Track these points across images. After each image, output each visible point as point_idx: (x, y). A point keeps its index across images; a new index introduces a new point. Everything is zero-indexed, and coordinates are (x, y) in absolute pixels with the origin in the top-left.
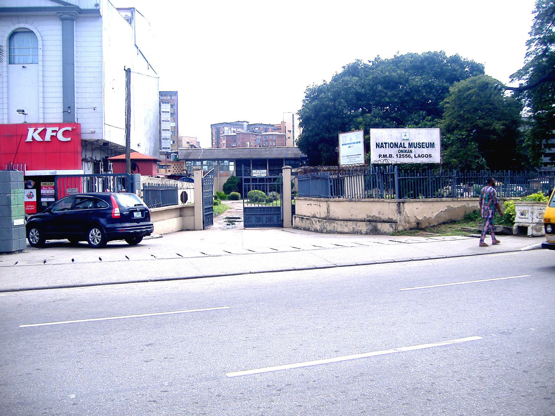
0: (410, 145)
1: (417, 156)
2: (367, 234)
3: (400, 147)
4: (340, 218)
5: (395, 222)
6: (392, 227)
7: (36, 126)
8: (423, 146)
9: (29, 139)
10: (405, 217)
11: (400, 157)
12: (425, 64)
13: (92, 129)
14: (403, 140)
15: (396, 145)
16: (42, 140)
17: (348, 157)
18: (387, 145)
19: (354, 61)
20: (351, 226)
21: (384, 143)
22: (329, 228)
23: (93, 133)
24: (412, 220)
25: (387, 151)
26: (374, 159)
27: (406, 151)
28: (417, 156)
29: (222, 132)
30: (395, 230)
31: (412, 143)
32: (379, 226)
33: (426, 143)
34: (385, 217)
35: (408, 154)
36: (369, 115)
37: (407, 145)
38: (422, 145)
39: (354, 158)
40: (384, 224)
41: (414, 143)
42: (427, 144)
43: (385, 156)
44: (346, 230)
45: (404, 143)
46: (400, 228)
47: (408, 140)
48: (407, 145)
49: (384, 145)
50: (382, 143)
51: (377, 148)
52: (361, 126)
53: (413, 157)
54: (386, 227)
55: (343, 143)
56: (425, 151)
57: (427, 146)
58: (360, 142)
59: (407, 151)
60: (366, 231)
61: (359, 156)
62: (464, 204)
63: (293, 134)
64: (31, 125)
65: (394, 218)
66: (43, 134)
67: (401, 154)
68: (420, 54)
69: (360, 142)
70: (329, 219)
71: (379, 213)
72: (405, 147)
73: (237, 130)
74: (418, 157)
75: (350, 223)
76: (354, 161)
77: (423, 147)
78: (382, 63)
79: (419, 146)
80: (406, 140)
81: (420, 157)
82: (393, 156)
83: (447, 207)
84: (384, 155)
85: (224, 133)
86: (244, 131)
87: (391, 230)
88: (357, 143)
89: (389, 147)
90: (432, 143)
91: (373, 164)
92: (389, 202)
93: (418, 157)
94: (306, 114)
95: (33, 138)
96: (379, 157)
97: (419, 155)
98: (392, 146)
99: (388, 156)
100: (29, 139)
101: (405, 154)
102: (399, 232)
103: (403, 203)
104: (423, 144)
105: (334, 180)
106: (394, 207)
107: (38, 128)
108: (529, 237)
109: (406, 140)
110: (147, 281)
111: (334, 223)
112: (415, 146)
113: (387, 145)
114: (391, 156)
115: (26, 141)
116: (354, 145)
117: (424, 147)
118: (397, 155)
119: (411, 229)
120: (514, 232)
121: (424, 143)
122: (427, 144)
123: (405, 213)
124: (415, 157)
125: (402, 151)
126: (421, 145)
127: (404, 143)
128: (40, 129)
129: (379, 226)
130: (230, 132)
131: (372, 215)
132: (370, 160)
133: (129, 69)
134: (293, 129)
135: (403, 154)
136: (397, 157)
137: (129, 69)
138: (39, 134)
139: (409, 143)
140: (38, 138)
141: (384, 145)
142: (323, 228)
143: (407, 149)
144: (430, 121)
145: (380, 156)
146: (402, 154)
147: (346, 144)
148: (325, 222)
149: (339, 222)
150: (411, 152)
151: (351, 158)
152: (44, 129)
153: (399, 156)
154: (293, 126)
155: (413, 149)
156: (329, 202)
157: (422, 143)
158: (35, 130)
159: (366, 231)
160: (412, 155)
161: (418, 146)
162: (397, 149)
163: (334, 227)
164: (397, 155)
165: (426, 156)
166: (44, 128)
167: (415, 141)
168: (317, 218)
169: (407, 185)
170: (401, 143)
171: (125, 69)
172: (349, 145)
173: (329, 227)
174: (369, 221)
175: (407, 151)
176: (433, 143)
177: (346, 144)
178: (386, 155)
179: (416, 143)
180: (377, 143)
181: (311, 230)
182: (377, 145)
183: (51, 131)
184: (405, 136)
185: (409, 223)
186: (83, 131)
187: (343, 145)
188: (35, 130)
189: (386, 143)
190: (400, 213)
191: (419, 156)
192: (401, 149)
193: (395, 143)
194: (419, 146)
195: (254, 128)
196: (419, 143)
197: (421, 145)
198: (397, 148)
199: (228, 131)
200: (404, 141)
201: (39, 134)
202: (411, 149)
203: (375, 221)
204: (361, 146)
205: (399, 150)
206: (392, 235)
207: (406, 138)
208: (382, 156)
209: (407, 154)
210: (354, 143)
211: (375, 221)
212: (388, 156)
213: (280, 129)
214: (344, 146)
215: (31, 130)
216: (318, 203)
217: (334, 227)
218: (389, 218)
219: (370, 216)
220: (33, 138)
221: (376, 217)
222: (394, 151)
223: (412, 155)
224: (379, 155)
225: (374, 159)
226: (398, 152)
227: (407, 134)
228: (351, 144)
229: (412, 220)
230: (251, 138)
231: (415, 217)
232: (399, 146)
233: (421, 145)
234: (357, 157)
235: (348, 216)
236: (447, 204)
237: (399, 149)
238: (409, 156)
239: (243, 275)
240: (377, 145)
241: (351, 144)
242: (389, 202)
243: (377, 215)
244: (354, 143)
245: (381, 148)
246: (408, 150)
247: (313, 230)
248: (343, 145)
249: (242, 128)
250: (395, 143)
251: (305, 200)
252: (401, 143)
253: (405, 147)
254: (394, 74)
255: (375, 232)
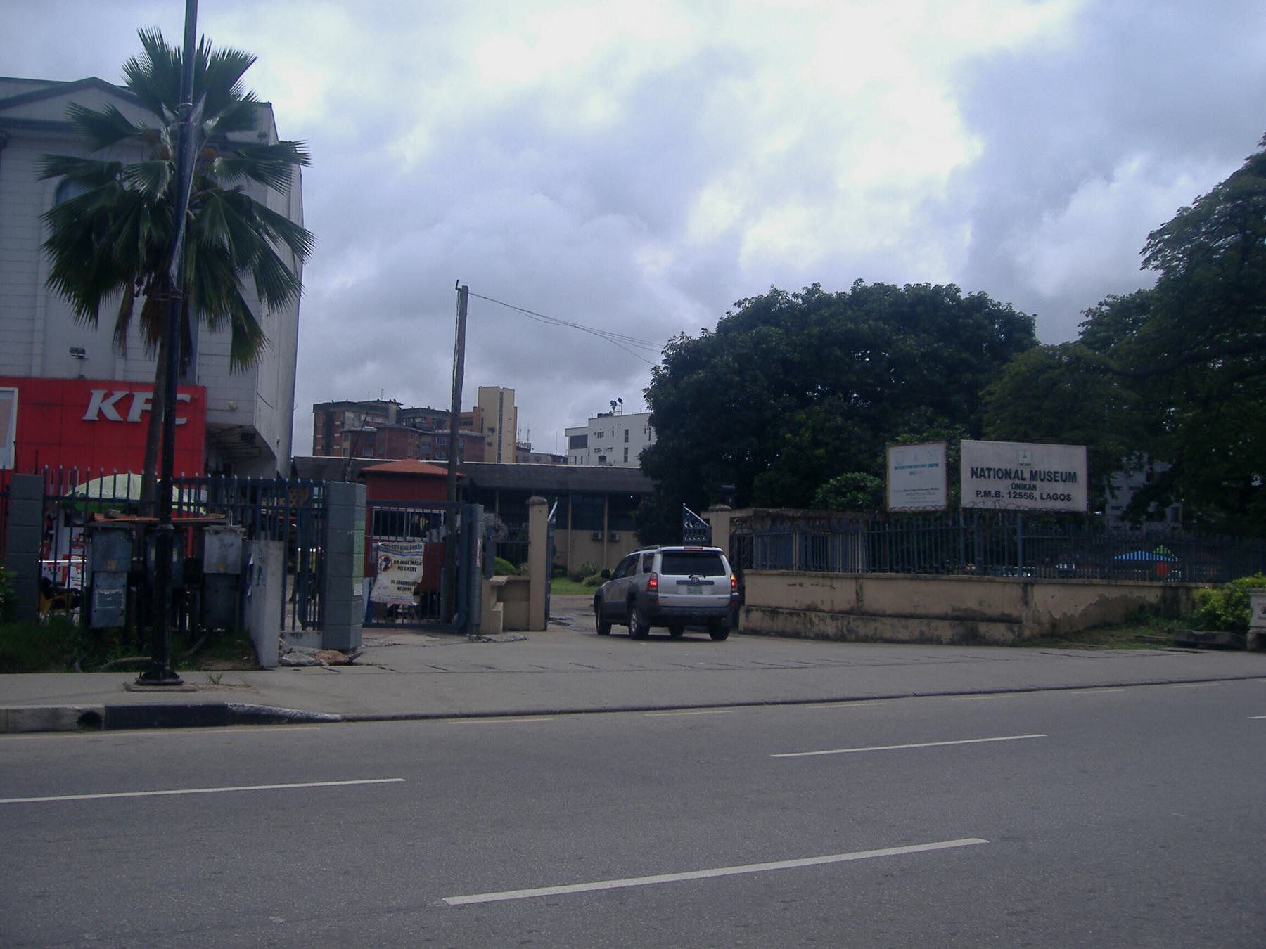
0: (1034, 475)
1: (1045, 497)
2: (953, 643)
3: (1015, 477)
4: (889, 612)
5: (1018, 621)
6: (1013, 631)
7: (109, 386)
8: (1057, 478)
9: (91, 414)
10: (1034, 612)
11: (1014, 497)
12: (920, 309)
13: (231, 402)
14: (1021, 464)
15: (1007, 474)
16: (122, 420)
17: (909, 492)
18: (992, 473)
19: (766, 292)
20: (915, 627)
21: (987, 469)
22: (862, 631)
23: (232, 410)
24: (1045, 618)
25: (992, 485)
26: (967, 499)
27: (1025, 487)
28: (1045, 497)
29: (339, 423)
30: (1019, 636)
31: (1036, 471)
32: (983, 628)
33: (1062, 473)
34: (994, 611)
35: (1029, 492)
36: (817, 408)
37: (1026, 475)
38: (1055, 477)
39: (922, 494)
40: (992, 626)
41: (1040, 472)
42: (1042, 473)
43: (987, 494)
44: (904, 635)
45: (1022, 471)
46: (1027, 633)
47: (1030, 465)
48: (1026, 475)
49: (986, 473)
50: (982, 470)
51: (972, 477)
52: (803, 429)
53: (1039, 498)
54: (999, 631)
55: (897, 465)
56: (1059, 488)
57: (1064, 478)
58: (937, 465)
59: (1027, 486)
60: (951, 637)
61: (933, 491)
62: (1126, 592)
63: (500, 437)
64: (98, 384)
65: (1015, 613)
66: (124, 405)
67: (1016, 491)
68: (901, 287)
69: (937, 465)
70: (860, 612)
71: (981, 603)
72: (1024, 479)
73: (373, 419)
74: (1047, 498)
75: (913, 623)
76: (919, 502)
77: (1056, 481)
78: (827, 301)
79: (1049, 479)
80: (1026, 465)
81: (1050, 498)
82: (1001, 495)
83: (1100, 595)
84: (985, 492)
85: (343, 424)
86: (392, 421)
87: (1010, 637)
88: (931, 466)
89: (994, 478)
90: (1034, 472)
91: (963, 508)
92: (1005, 583)
93: (1047, 498)
94: (672, 398)
95: (100, 413)
96: (977, 496)
97: (1049, 495)
98: (1000, 475)
99: (993, 493)
100: (91, 414)
101: (1023, 491)
102: (1024, 640)
103: (1032, 584)
104: (1057, 475)
105: (823, 538)
106: (1016, 592)
107: (114, 392)
108: (547, 581)
109: (1026, 465)
110: (762, 704)
111: (875, 620)
112: (1042, 477)
113: (992, 473)
114: (998, 494)
115: (84, 418)
116: (923, 469)
117: (1058, 481)
118: (1009, 493)
119: (1043, 636)
120: (1248, 645)
121: (1058, 472)
122: (1042, 473)
123: (1033, 605)
124: (1042, 498)
125: (1018, 486)
126: (1052, 475)
127: (1022, 471)
128: (119, 395)
129: (983, 628)
130: (357, 423)
131: (964, 606)
132: (959, 499)
133: (465, 288)
134: (501, 424)
135: (1021, 491)
136: (1010, 497)
137: (465, 288)
138: (116, 405)
139: (1031, 472)
140: (112, 414)
141: (986, 473)
142: (848, 631)
143: (1028, 482)
144: (946, 427)
145: (978, 493)
146: (1018, 491)
147: (903, 468)
148: (854, 620)
149: (888, 621)
150: (1034, 488)
151: (914, 494)
152: (127, 395)
153: (1012, 495)
154: (501, 420)
155: (1038, 483)
156: (861, 581)
157: (1055, 473)
158: (106, 397)
159: (951, 637)
160: (1037, 494)
161: (1047, 477)
162: (1009, 482)
163: (876, 629)
164: (1009, 493)
165: (1062, 497)
166: (128, 392)
167: (1042, 467)
168: (824, 611)
169: (922, 556)
170: (1017, 471)
171: (458, 287)
172: (913, 470)
173: (864, 629)
174: (957, 618)
175: (1027, 486)
176: (1075, 473)
177: (903, 468)
178: (990, 492)
179: (1044, 472)
180: (972, 469)
181: (804, 635)
182: (974, 473)
183: (144, 400)
184: (1025, 457)
185: (1040, 623)
186: (211, 404)
187: (896, 468)
188: (106, 397)
189: (989, 470)
190: (1026, 603)
191: (1049, 497)
192: (1017, 481)
193: (1006, 470)
194: (1049, 479)
195: (414, 418)
196: (1048, 472)
197: (1052, 477)
198: (1010, 478)
199: (351, 421)
200: (1021, 467)
201: (116, 405)
202: (1035, 483)
203: (973, 619)
204: (940, 474)
205: (1014, 483)
206: (1014, 645)
207: (1025, 461)
208: (983, 494)
209: (1027, 491)
210: (923, 466)
211: (973, 619)
212: (993, 493)
213: (471, 423)
214: (898, 470)
215: (97, 396)
216: (828, 582)
217: (876, 629)
218: (1003, 614)
219: (959, 610)
220: (100, 413)
221: (974, 612)
222: (1003, 485)
223: (1037, 494)
224: (977, 491)
225: (967, 499)
226: (1010, 488)
227: (1028, 454)
228: (915, 467)
229: (1045, 618)
230: (409, 441)
231: (1049, 612)
232: (979, 475)
233: (1052, 475)
234: (930, 494)
235: (908, 608)
236: (1100, 591)
237: (1013, 481)
238: (1031, 497)
239: (905, 699)
240: (974, 473)
241: (915, 467)
242: (1005, 583)
243: (975, 607)
244: (923, 466)
245: (980, 477)
246: (1030, 485)
247: (812, 635)
248: (896, 468)
249: (386, 416)
250: (1006, 470)
251: (783, 575)
252: (1017, 471)
253: (1024, 479)
254: (864, 326)
255: (972, 638)
